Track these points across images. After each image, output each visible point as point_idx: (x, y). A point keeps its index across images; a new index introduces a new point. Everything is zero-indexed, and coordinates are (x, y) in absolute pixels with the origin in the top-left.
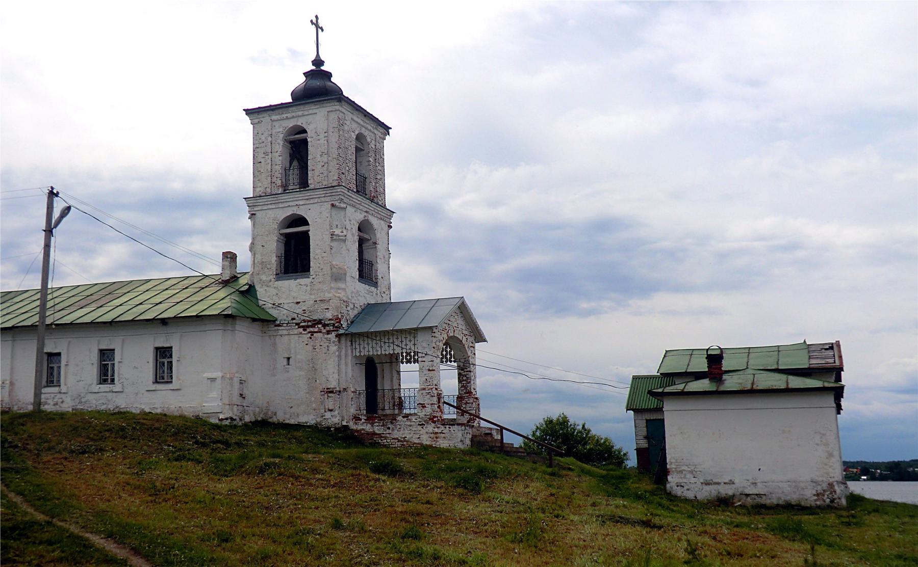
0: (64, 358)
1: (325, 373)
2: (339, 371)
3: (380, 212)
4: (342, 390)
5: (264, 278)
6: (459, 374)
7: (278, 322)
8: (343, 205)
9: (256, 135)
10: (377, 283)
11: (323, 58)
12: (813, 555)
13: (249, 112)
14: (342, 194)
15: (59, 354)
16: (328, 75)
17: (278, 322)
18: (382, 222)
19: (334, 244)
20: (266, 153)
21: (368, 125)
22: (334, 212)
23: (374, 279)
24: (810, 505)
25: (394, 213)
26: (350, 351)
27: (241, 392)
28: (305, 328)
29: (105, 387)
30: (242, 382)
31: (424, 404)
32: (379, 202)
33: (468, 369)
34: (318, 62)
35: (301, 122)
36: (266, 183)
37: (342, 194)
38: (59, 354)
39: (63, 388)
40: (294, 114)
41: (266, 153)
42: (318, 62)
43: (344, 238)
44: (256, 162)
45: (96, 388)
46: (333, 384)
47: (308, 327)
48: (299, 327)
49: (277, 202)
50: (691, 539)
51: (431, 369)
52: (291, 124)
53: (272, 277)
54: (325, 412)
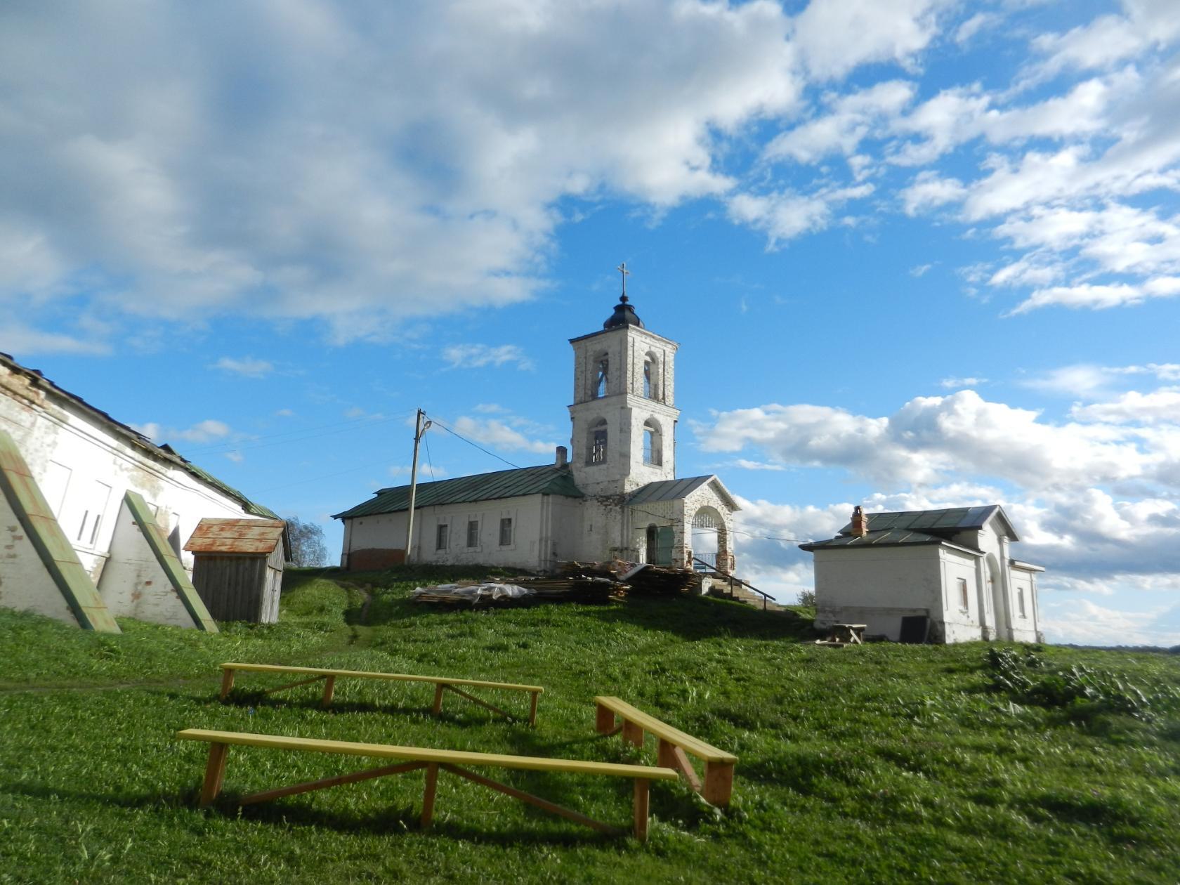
0: (449, 528)
1: (613, 536)
2: (622, 536)
5: (578, 465)
6: (719, 537)
7: (648, 359)
9: (577, 358)
11: (626, 295)
12: (688, 861)
13: (572, 341)
15: (446, 526)
16: (630, 308)
17: (648, 359)
18: (669, 418)
20: (582, 372)
24: (1039, 636)
29: (471, 549)
30: (554, 544)
34: (624, 299)
36: (582, 394)
38: (446, 526)
39: (448, 550)
41: (582, 372)
42: (624, 299)
44: (576, 379)
45: (466, 550)
46: (618, 545)
47: (604, 501)
50: (617, 856)
53: (583, 465)
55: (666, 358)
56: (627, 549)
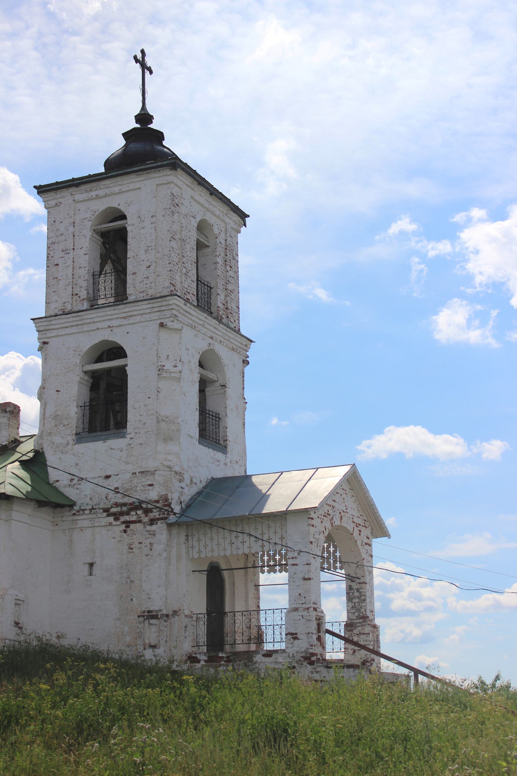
3: (231, 340)
4: (171, 613)
5: (58, 440)
6: (350, 588)
8: (176, 325)
10: (226, 447)
14: (176, 308)
19: (163, 384)
21: (215, 209)
22: (164, 333)
23: (221, 442)
25: (252, 341)
26: (184, 551)
27: (17, 620)
28: (116, 516)
30: (18, 603)
31: (296, 634)
32: (230, 324)
33: (362, 580)
35: (114, 202)
37: (176, 308)
40: (107, 191)
43: (178, 375)
46: (155, 606)
48: (108, 515)
49: (80, 323)
51: (307, 577)
52: (101, 206)
54: (145, 649)
55: (229, 239)
56: (175, 613)
